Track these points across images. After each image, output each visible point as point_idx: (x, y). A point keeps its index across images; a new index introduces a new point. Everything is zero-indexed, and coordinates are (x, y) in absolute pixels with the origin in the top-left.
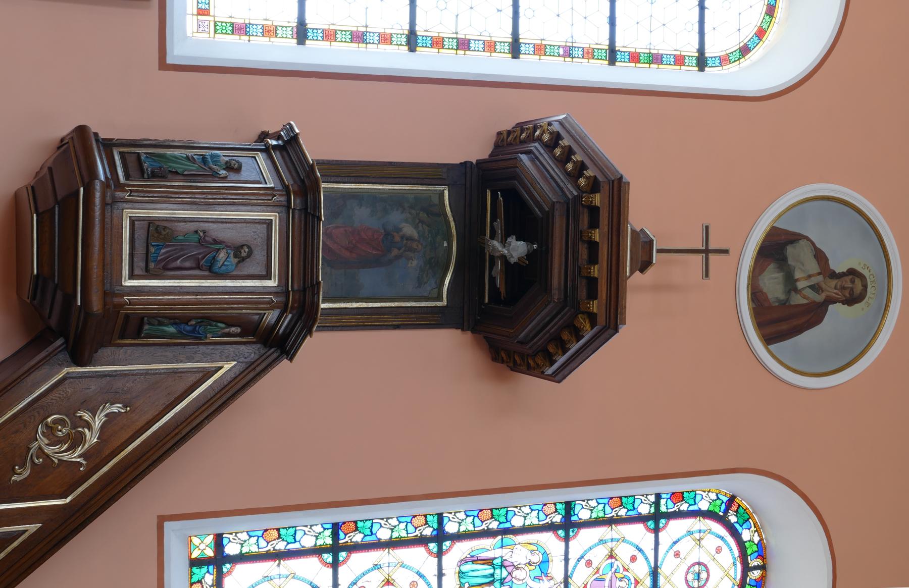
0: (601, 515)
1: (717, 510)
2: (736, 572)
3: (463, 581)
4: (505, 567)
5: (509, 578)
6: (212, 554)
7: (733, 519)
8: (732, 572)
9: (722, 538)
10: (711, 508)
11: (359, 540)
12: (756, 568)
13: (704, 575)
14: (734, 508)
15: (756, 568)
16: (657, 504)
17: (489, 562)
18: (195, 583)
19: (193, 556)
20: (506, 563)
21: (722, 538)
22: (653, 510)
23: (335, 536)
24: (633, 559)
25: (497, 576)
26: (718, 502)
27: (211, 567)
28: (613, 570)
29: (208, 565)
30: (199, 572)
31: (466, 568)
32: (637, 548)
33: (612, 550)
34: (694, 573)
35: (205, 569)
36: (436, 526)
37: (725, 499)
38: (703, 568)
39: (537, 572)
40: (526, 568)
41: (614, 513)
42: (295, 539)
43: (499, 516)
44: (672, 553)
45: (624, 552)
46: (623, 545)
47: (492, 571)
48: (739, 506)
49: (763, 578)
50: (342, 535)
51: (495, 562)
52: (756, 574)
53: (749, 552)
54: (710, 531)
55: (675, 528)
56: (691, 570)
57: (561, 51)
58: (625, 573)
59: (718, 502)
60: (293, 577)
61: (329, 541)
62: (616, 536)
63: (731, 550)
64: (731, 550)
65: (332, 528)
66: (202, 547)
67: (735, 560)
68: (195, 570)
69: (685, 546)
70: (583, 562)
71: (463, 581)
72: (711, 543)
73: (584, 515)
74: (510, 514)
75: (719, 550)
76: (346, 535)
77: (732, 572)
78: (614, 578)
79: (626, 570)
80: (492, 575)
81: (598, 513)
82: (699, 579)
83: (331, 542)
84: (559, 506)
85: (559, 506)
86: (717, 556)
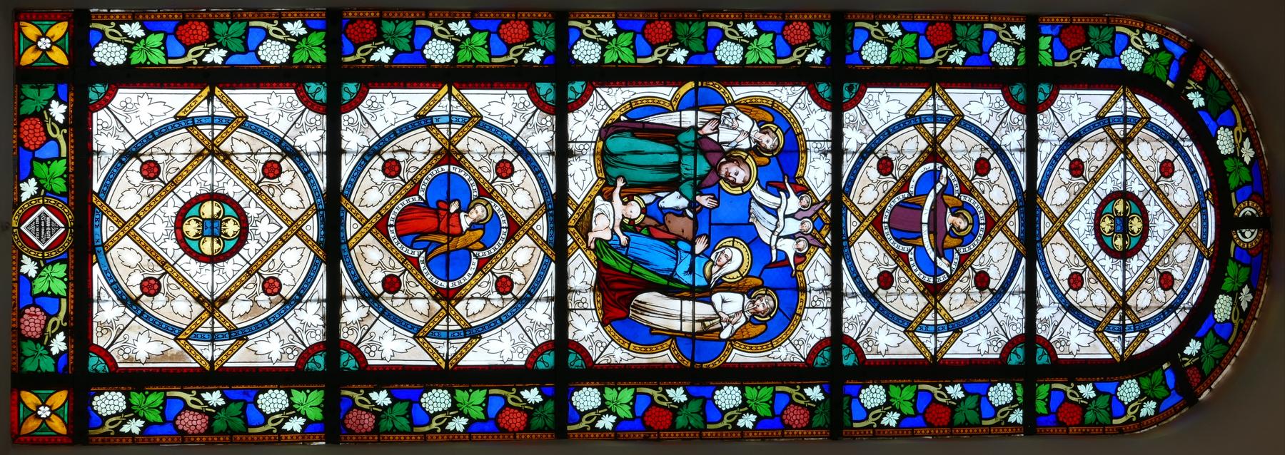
0: (911, 58)
1: (1161, 74)
3: (613, 172)
4: (704, 153)
5: (713, 177)
7: (1197, 100)
9: (1173, 142)
10: (1149, 69)
11: (219, 61)
12: (1248, 222)
13: (1136, 225)
14: (1200, 71)
15: (1248, 222)
16: (1030, 45)
17: (668, 135)
18: (27, 116)
20: (706, 146)
21: (1173, 142)
22: (1022, 60)
24: (982, 167)
25: (687, 170)
26: (1164, 57)
27: (63, 88)
28: (939, 187)
30: (34, 97)
31: (619, 144)
32: (514, 143)
34: (1115, 217)
35: (48, 92)
37: (1178, 51)
38: (1135, 208)
39: (774, 173)
40: (750, 161)
41: (190, 58)
42: (245, 44)
43: (689, 36)
44: (1064, 163)
45: (961, 147)
46: (958, 133)
47: (675, 158)
49: (1264, 245)
51: (683, 138)
52: (1248, 236)
53: (1233, 182)
54: (1146, 121)
55: (1077, 107)
56: (1108, 208)
58: (966, 198)
59: (1164, 57)
60: (476, 126)
61: (320, 56)
62: (221, 110)
63: (1193, 172)
64: (1193, 172)
66: (44, 44)
68: (29, 91)
69: (1095, 151)
70: (873, 161)
71: (613, 172)
72: (1147, 150)
74: (988, 37)
75: (1167, 169)
78: (940, 206)
79: (964, 190)
80: (676, 167)
83: (324, 59)
84: (819, 29)
85: (819, 29)
86: (166, 176)
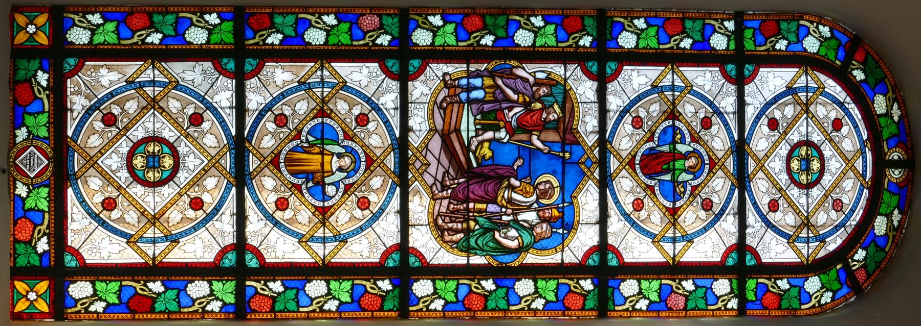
2: (864, 161)
6: (234, 283)
8: (859, 165)
9: (841, 105)
13: (816, 165)
19: (16, 42)
21: (841, 105)
23: (239, 33)
29: (154, 182)
33: (673, 103)
34: (801, 160)
36: (396, 32)
44: (764, 120)
48: (868, 54)
50: (249, 33)
52: (895, 174)
53: (886, 134)
55: (772, 80)
57: (142, 210)
61: (229, 38)
64: (856, 127)
65: (234, 12)
67: (863, 143)
73: (627, 40)
75: (837, 125)
76: (255, 33)
77: (859, 165)
81: (651, 42)
82: (808, 170)
